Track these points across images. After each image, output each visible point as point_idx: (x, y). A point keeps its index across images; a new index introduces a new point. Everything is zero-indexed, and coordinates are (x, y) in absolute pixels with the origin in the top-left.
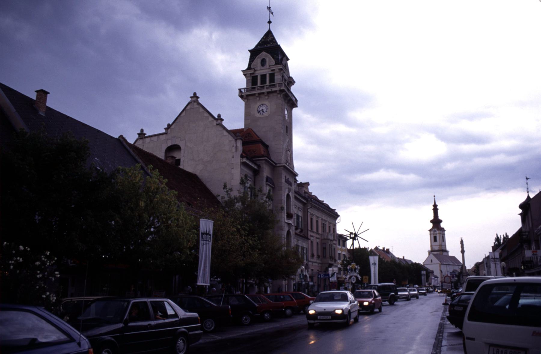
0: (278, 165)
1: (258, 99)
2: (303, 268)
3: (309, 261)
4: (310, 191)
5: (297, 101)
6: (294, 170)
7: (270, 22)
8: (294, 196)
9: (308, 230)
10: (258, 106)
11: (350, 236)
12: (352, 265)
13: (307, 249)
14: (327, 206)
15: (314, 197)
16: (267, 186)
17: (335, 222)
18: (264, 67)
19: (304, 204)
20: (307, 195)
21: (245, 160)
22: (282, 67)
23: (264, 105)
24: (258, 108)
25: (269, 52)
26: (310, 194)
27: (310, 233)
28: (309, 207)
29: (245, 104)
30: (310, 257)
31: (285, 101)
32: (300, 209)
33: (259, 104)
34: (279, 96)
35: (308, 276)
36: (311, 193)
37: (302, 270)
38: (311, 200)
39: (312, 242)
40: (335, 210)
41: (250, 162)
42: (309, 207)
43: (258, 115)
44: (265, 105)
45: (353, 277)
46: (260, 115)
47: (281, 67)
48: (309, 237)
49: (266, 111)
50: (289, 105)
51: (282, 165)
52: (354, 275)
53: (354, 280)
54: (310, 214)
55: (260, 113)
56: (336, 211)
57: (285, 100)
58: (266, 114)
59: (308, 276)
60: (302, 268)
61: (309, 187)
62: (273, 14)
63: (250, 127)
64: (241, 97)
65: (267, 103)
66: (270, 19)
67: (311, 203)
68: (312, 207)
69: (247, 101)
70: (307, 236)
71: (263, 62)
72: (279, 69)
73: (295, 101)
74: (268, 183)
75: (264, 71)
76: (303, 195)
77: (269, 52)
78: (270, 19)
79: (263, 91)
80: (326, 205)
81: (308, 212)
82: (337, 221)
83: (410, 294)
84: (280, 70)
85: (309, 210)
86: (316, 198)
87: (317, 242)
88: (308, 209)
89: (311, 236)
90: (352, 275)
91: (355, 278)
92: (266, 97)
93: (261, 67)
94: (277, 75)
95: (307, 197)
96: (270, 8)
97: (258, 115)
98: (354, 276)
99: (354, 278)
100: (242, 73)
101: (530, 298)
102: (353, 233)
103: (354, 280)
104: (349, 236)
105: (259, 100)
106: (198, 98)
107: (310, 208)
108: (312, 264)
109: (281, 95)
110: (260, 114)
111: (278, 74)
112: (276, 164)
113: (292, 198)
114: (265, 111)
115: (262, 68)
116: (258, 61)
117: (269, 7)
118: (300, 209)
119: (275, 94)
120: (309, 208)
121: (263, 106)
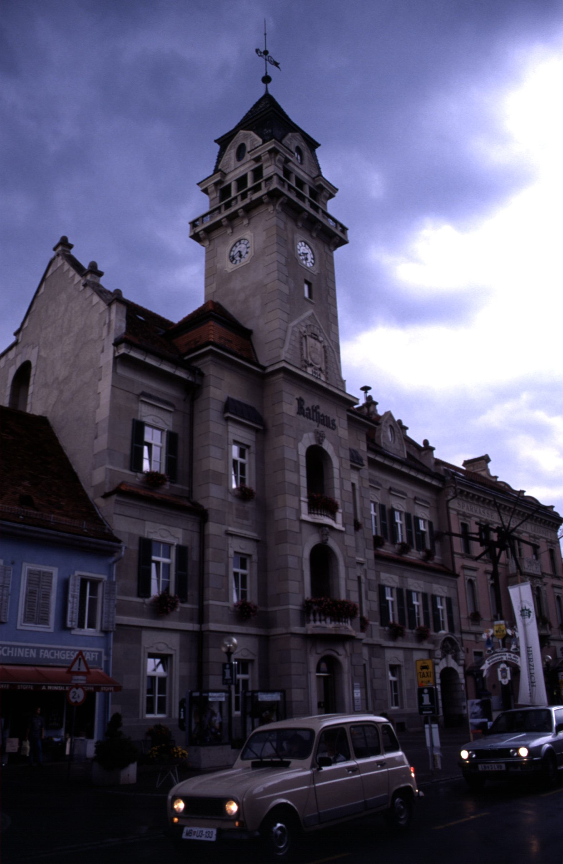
0: (270, 369)
1: (229, 231)
2: (548, 658)
3: (462, 632)
4: (493, 474)
5: (344, 229)
6: (344, 392)
7: (267, 79)
8: (346, 454)
9: (453, 553)
10: (230, 248)
11: (481, 536)
12: (496, 628)
13: (449, 601)
14: (534, 501)
15: (503, 485)
16: (230, 423)
17: (556, 536)
18: (243, 161)
19: (437, 491)
20: (442, 468)
21: (123, 350)
22: (275, 143)
23: (242, 242)
24: (231, 251)
25: (254, 128)
26: (494, 480)
27: (459, 562)
28: (449, 497)
29: (207, 252)
30: (464, 621)
31: (297, 226)
32: (417, 502)
33: (231, 242)
34: (271, 208)
35: (460, 670)
36: (496, 477)
37: (229, 648)
38: (454, 479)
39: (471, 582)
40: (552, 507)
41: (176, 369)
42: (449, 497)
43: (230, 267)
44: (245, 239)
45: (503, 666)
46: (235, 265)
47: (273, 146)
48: (458, 570)
49: (247, 253)
50: (314, 235)
51: (277, 367)
52: (504, 658)
53: (504, 677)
54: (458, 514)
55: (234, 262)
56: (555, 510)
57: (295, 221)
58: (246, 260)
59: (460, 670)
60: (547, 660)
61: (490, 465)
62: (279, 66)
63: (216, 300)
64: (196, 237)
65: (248, 235)
66: (266, 73)
67: (454, 485)
68: (459, 494)
69: (210, 245)
70: (451, 568)
71: (241, 152)
72: (270, 152)
73: (336, 227)
74: (228, 415)
75: (242, 169)
76: (433, 470)
77: (254, 128)
78: (266, 73)
79: (233, 209)
80: (531, 500)
81: (448, 508)
82: (559, 533)
83: (272, 760)
84: (273, 155)
85: (451, 505)
86: (507, 487)
87: (557, 595)
88: (448, 501)
89: (464, 567)
90: (496, 658)
91: (508, 669)
92: (246, 222)
93: (237, 162)
94: (267, 167)
95: (442, 473)
96: (266, 52)
97: (230, 267)
98: (506, 662)
99: (504, 670)
100: (199, 189)
101: (132, 502)
102: (495, 526)
103: (504, 677)
104: (478, 537)
105: (232, 233)
106: (71, 246)
107: (453, 498)
108: (476, 638)
109: (274, 206)
110: (235, 263)
111: (269, 164)
112: (264, 368)
113: (335, 462)
114: (243, 253)
115: (239, 164)
116: (231, 153)
117: (262, 50)
118: (417, 502)
119: (262, 209)
120: (451, 499)
121: (240, 244)
